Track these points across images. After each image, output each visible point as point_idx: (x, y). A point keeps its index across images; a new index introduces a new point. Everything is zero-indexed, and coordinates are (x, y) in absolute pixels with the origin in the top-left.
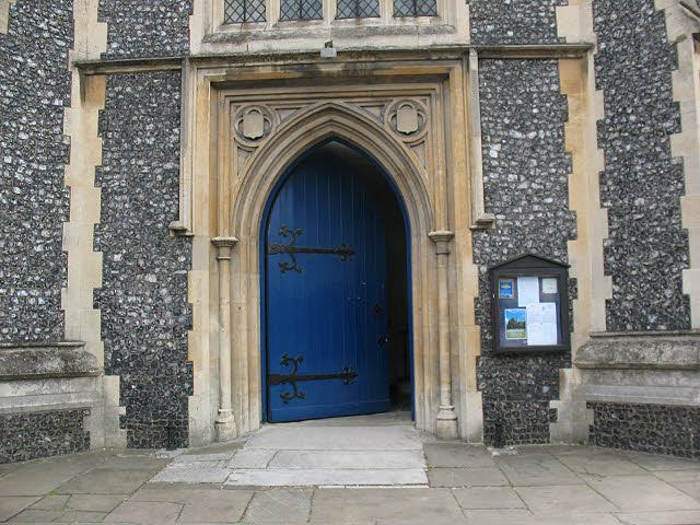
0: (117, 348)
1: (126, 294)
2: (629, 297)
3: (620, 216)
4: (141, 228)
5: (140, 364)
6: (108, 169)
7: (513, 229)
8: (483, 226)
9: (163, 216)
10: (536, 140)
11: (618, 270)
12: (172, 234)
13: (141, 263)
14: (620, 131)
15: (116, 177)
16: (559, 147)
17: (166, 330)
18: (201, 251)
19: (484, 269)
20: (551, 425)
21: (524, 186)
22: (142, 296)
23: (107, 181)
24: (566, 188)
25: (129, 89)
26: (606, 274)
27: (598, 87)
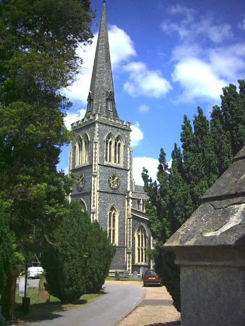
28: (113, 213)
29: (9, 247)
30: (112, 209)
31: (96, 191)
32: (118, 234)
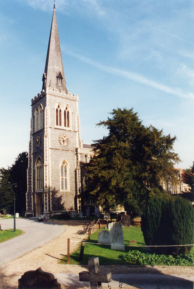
18: (36, 205)
28: (64, 166)
29: (42, 103)
30: (64, 162)
31: (47, 149)
32: (69, 187)
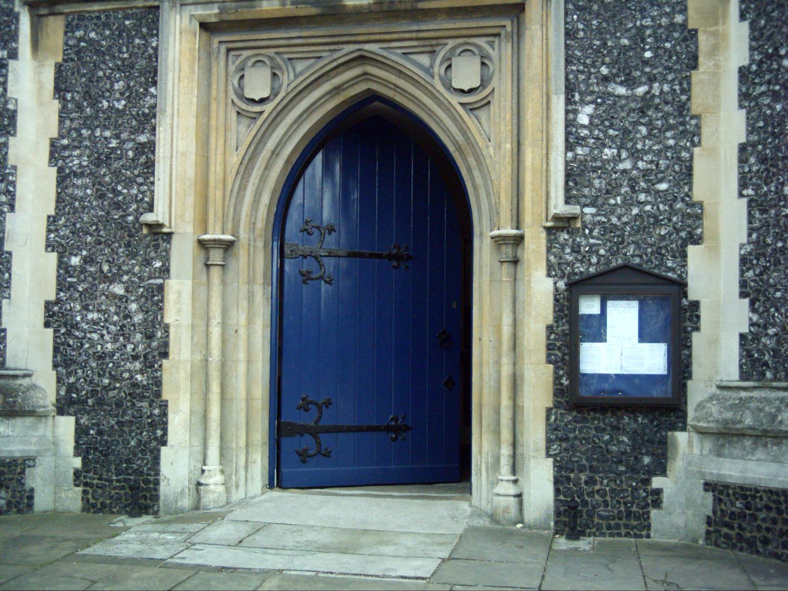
0: (72, 380)
1: (86, 308)
2: (771, 331)
3: (764, 211)
4: (107, 220)
5: (100, 402)
6: (65, 142)
7: (607, 229)
8: (563, 223)
9: (134, 206)
10: (648, 99)
11: (758, 291)
12: (145, 231)
13: (106, 268)
14: (769, 82)
15: (76, 153)
16: (682, 109)
17: (135, 358)
19: (561, 284)
20: (654, 513)
21: (627, 165)
22: (105, 312)
23: (64, 159)
24: (690, 169)
25: (93, 35)
26: (743, 295)
27: (742, 17)
